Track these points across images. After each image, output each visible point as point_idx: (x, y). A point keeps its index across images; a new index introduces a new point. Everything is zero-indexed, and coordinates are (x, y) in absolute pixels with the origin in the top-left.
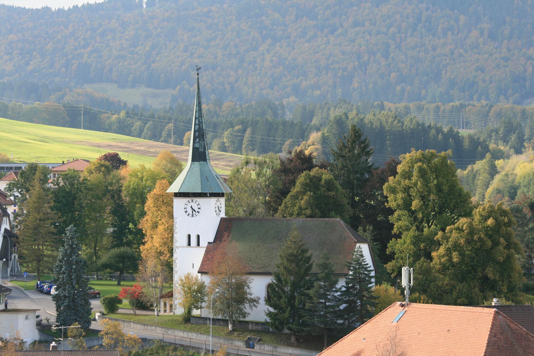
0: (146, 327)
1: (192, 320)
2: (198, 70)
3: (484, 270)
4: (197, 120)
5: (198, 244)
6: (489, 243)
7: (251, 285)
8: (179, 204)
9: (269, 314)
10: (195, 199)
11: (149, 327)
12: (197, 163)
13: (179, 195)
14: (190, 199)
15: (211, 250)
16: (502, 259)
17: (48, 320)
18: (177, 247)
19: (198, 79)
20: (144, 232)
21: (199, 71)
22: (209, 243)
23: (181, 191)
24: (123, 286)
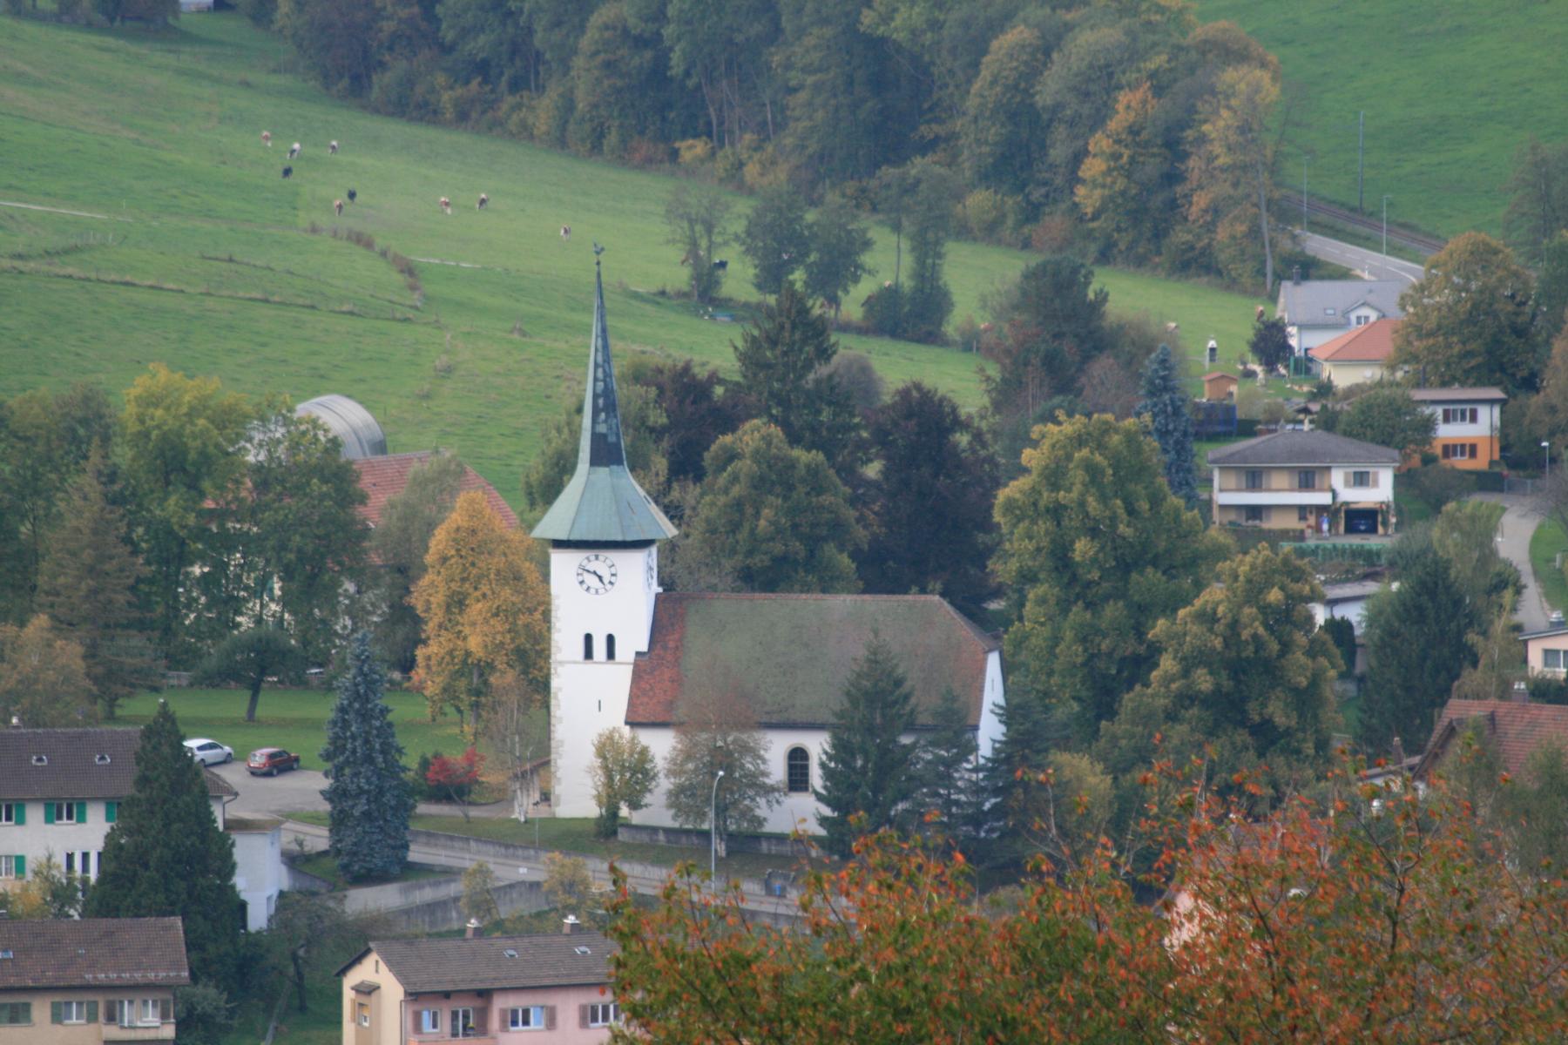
0: (511, 851)
1: (623, 836)
2: (598, 253)
3: (1264, 705)
4: (600, 371)
5: (611, 655)
6: (1274, 647)
7: (767, 756)
8: (563, 565)
9: (823, 821)
10: (603, 554)
11: (520, 852)
12: (603, 471)
13: (560, 544)
14: (591, 554)
15: (643, 667)
16: (1303, 682)
17: (301, 844)
18: (561, 663)
19: (599, 275)
20: (419, 611)
21: (602, 257)
22: (638, 654)
23: (572, 538)
24: (283, 724)
